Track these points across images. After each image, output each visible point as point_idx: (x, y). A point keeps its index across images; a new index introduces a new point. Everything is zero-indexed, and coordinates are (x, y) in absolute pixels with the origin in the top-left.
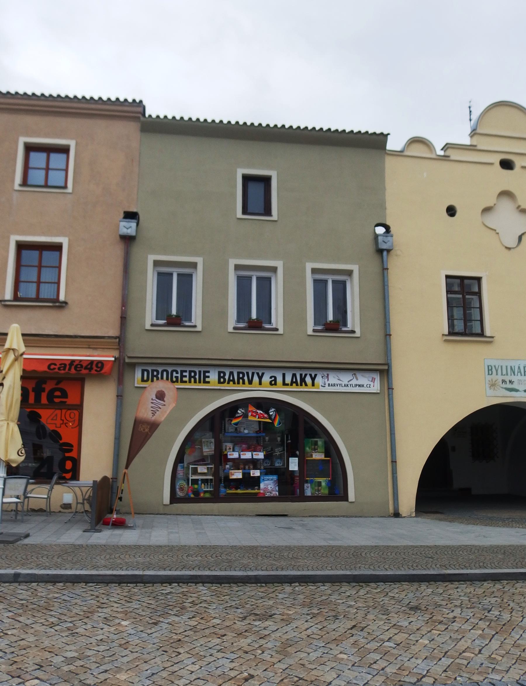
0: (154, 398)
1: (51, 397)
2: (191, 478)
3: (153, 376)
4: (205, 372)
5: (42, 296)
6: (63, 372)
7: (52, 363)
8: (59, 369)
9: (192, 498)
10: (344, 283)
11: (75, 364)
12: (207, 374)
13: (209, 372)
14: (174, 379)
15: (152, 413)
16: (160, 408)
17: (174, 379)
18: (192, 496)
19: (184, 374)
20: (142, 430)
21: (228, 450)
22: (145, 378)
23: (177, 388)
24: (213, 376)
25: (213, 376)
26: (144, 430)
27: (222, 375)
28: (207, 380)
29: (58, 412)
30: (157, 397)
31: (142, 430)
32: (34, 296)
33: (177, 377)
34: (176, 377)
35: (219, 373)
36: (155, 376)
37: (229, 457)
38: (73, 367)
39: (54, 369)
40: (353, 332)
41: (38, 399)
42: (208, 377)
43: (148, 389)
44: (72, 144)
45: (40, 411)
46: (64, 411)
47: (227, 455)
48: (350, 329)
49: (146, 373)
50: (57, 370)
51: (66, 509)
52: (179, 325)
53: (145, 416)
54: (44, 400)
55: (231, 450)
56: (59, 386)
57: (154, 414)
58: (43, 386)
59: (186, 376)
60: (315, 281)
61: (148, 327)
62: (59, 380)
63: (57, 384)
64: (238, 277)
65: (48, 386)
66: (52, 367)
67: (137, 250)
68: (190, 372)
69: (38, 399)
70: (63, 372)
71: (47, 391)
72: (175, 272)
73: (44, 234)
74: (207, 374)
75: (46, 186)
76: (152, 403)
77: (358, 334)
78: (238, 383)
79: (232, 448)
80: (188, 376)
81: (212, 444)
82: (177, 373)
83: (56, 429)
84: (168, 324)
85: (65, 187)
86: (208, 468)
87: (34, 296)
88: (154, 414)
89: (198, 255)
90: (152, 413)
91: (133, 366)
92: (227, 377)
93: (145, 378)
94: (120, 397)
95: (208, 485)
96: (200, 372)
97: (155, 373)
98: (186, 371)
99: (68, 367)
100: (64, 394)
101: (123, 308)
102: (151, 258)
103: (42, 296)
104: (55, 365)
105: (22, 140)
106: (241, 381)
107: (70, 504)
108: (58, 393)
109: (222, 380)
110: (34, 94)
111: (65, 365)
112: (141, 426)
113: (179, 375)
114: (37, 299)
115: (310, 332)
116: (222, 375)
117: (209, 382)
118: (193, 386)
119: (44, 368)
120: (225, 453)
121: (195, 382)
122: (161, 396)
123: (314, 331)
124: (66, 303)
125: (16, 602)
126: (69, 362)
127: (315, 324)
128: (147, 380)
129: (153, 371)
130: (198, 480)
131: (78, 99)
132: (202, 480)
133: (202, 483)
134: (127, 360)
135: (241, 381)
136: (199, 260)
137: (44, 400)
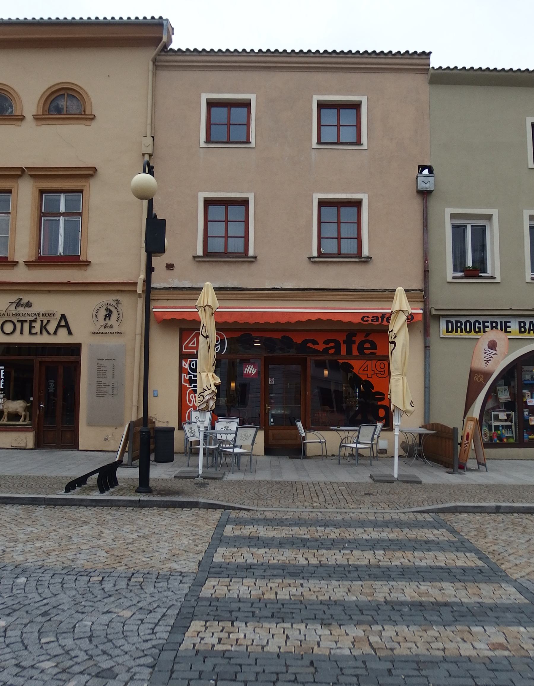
0: (487, 348)
1: (361, 349)
2: (493, 424)
3: (457, 327)
4: (506, 322)
5: (343, 252)
6: (376, 323)
7: (364, 316)
8: (372, 320)
9: (498, 443)
10: (483, 228)
11: (386, 317)
12: (508, 324)
13: (509, 322)
14: (477, 330)
15: (486, 363)
16: (492, 358)
17: (477, 330)
18: (498, 441)
19: (486, 324)
20: (477, 379)
21: (527, 398)
22: (450, 330)
23: (509, 339)
24: (514, 326)
25: (514, 326)
26: (479, 379)
27: (522, 325)
28: (508, 329)
29: (369, 362)
30: (489, 347)
31: (477, 379)
32: (335, 251)
33: (479, 328)
34: (478, 327)
35: (520, 323)
36: (459, 327)
37: (529, 404)
38: (385, 319)
39: (368, 321)
40: (494, 278)
41: (349, 351)
42: (509, 327)
43: (480, 340)
44: (364, 99)
45: (352, 363)
46: (374, 362)
47: (526, 402)
48: (490, 275)
49: (450, 324)
50: (370, 322)
51: (382, 454)
52: (477, 276)
53: (479, 366)
54: (355, 352)
55: (530, 397)
56: (368, 338)
57: (487, 364)
58: (354, 338)
59: (488, 327)
60: (454, 226)
61: (450, 279)
62: (368, 333)
63: (366, 336)
64: (452, 225)
65: (358, 339)
66: (366, 319)
67: (434, 203)
68: (492, 322)
69: (349, 351)
70: (376, 323)
71: (357, 343)
72: (469, 224)
73: (344, 191)
74: (508, 324)
75: (338, 143)
76: (485, 353)
77: (498, 280)
78: (457, 332)
79: (530, 395)
80: (490, 327)
81: (506, 391)
82: (480, 324)
83: (368, 379)
84: (466, 276)
85: (248, 142)
86: (507, 414)
87: (335, 251)
88: (487, 364)
89: (493, 207)
90: (486, 363)
91: (437, 318)
92: (527, 327)
93: (450, 330)
94: (426, 347)
95: (507, 430)
96: (501, 322)
97: (459, 324)
98: (488, 322)
99: (380, 319)
100: (374, 346)
101: (426, 262)
102: (448, 211)
103: (343, 252)
104: (368, 317)
105: (204, 97)
106: (459, 329)
107: (386, 449)
108: (367, 345)
109: (523, 330)
110: (228, 50)
111: (378, 318)
112: (476, 376)
113: (481, 326)
114: (339, 255)
115: (528, 280)
116: (522, 325)
117: (510, 332)
118: (459, 335)
119: (358, 320)
120: (525, 400)
121: (462, 332)
122: (493, 346)
123: (454, 277)
124: (255, 257)
125: (468, 539)
126: (381, 315)
127: (455, 270)
128: (452, 331)
129: (457, 322)
130: (499, 426)
131: (223, 52)
132: (502, 426)
133: (503, 428)
134: (434, 312)
135: (459, 329)
136: (494, 212)
137: (355, 352)
